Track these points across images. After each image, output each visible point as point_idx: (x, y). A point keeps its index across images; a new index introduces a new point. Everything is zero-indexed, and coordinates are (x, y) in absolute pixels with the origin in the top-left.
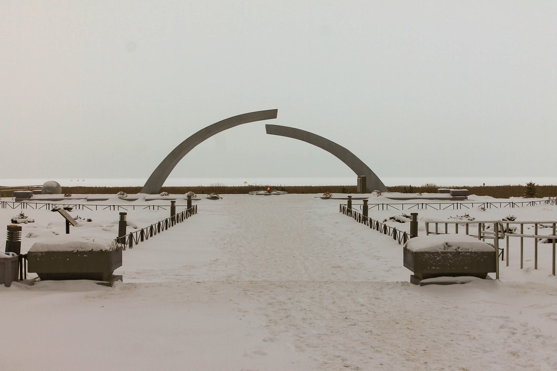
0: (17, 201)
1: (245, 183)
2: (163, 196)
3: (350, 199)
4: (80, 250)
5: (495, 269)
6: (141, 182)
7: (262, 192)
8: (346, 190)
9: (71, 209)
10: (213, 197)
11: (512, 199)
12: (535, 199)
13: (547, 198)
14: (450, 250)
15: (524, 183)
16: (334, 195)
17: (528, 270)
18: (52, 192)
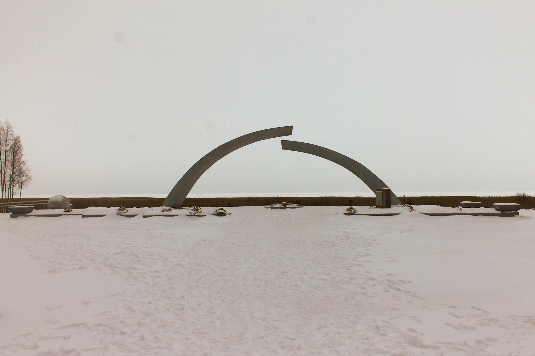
0: (12, 217)
2: (163, 211)
7: (278, 206)
8: (352, 202)
10: (219, 213)
16: (359, 209)
18: (56, 207)
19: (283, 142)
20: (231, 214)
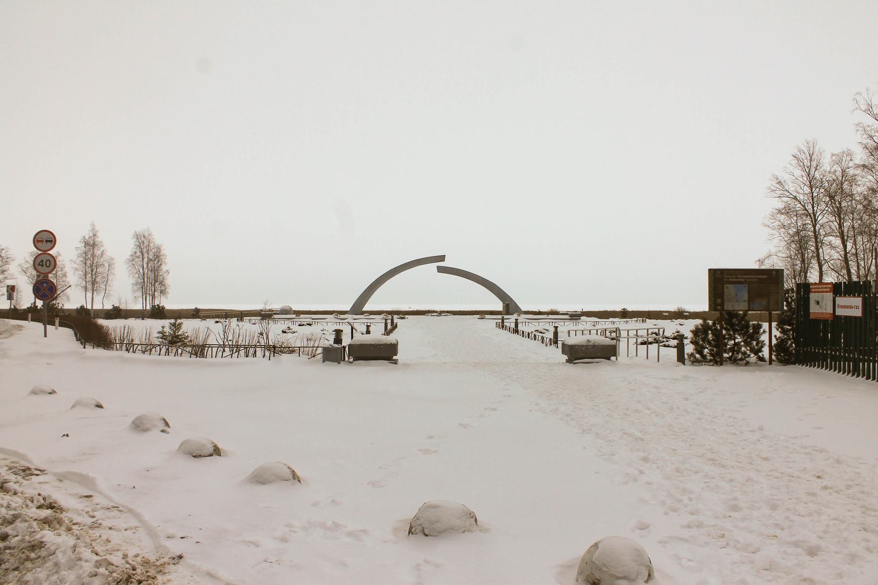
1: (410, 308)
3: (503, 320)
4: (379, 343)
5: (615, 355)
6: (347, 307)
9: (311, 324)
11: (611, 319)
12: (628, 320)
13: (636, 319)
14: (590, 344)
15: (618, 308)
16: (487, 317)
17: (632, 358)
19: (438, 267)
20: (132, 487)
